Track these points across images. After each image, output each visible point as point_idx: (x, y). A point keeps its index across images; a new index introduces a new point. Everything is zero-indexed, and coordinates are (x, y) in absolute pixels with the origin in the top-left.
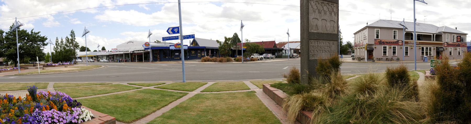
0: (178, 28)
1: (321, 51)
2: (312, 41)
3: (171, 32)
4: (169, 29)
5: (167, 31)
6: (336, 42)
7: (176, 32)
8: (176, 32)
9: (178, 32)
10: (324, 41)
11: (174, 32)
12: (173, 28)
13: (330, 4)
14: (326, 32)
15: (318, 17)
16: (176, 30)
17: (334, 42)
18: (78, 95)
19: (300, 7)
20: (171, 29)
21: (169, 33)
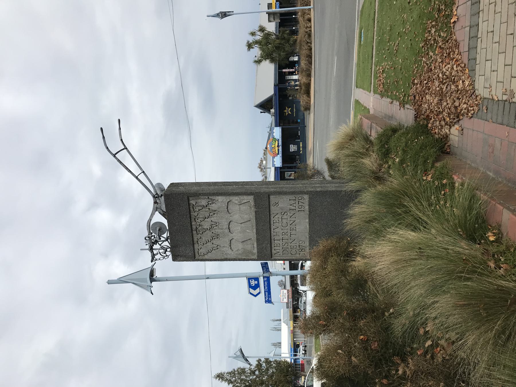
0: (249, 279)
1: (293, 232)
2: (273, 252)
3: (258, 291)
4: (251, 294)
5: (255, 296)
6: (272, 197)
7: (256, 282)
8: (256, 282)
9: (257, 279)
10: (273, 227)
11: (257, 286)
12: (250, 286)
13: (194, 214)
14: (254, 221)
15: (227, 240)
16: (253, 283)
17: (271, 203)
18: (316, 77)
19: (193, 181)
20: (252, 291)
21: (259, 293)
